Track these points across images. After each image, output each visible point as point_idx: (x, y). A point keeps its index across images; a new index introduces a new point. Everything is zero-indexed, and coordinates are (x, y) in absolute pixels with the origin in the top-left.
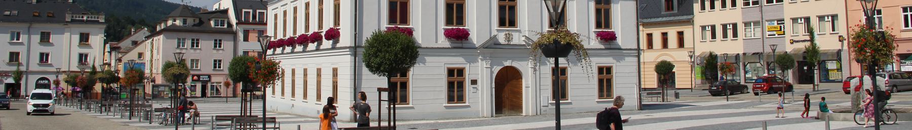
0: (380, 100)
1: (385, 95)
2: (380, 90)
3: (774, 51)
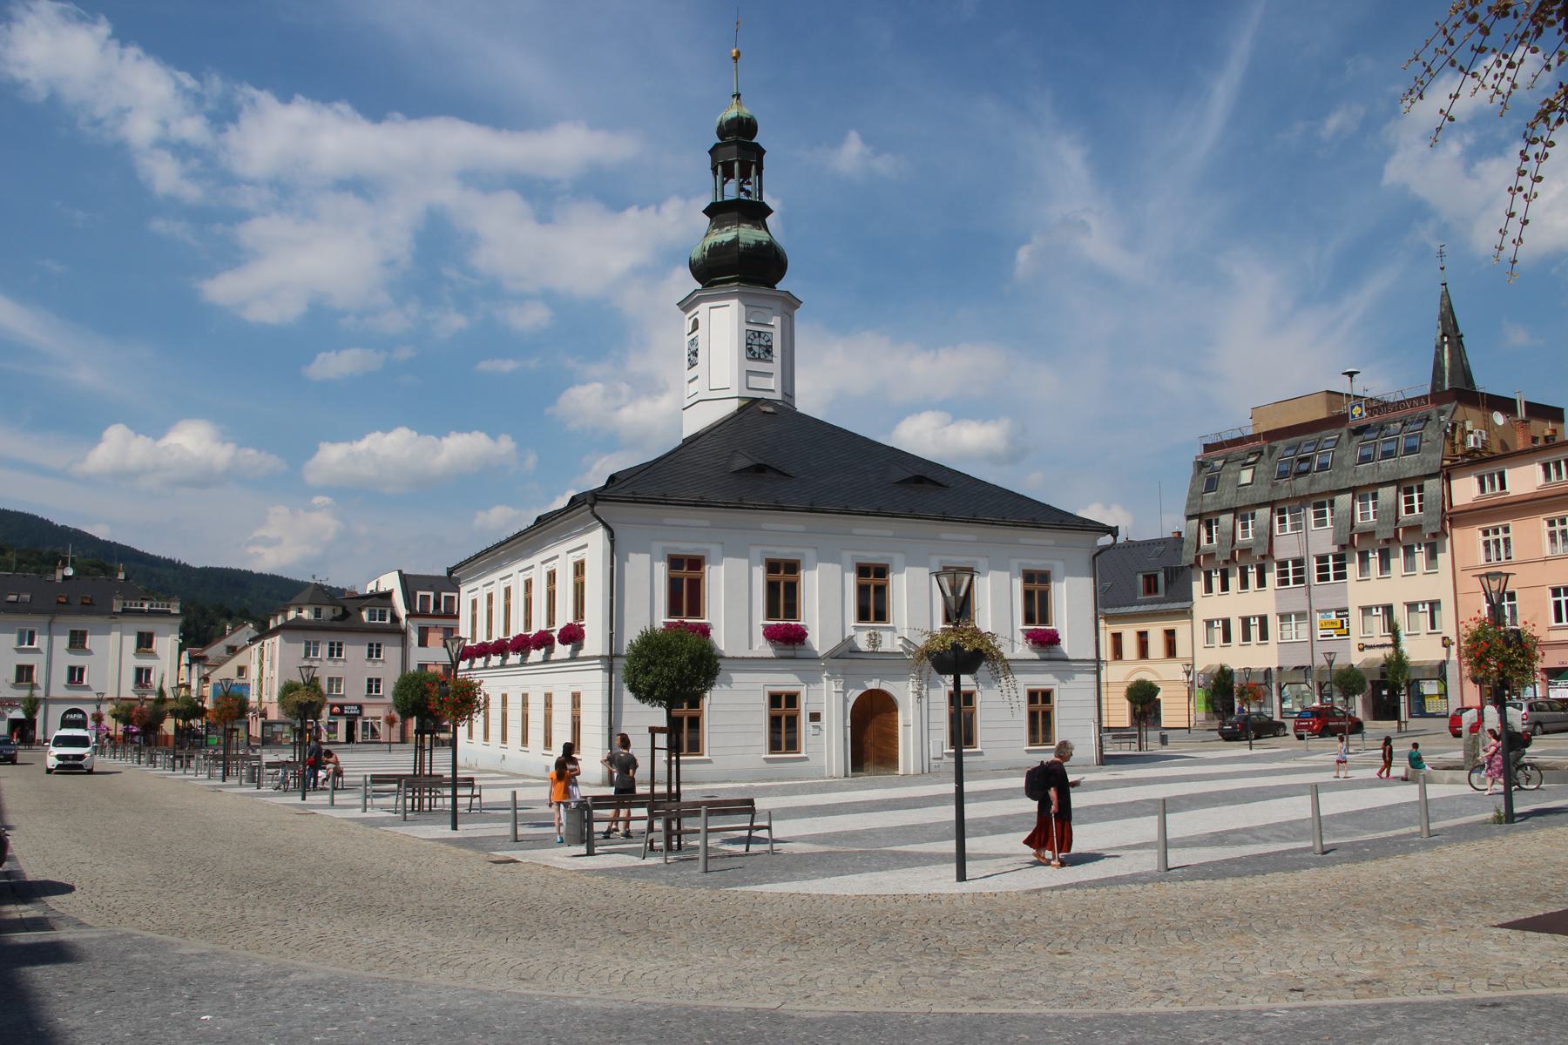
0: (653, 748)
1: (662, 740)
2: (653, 731)
3: (1330, 663)
